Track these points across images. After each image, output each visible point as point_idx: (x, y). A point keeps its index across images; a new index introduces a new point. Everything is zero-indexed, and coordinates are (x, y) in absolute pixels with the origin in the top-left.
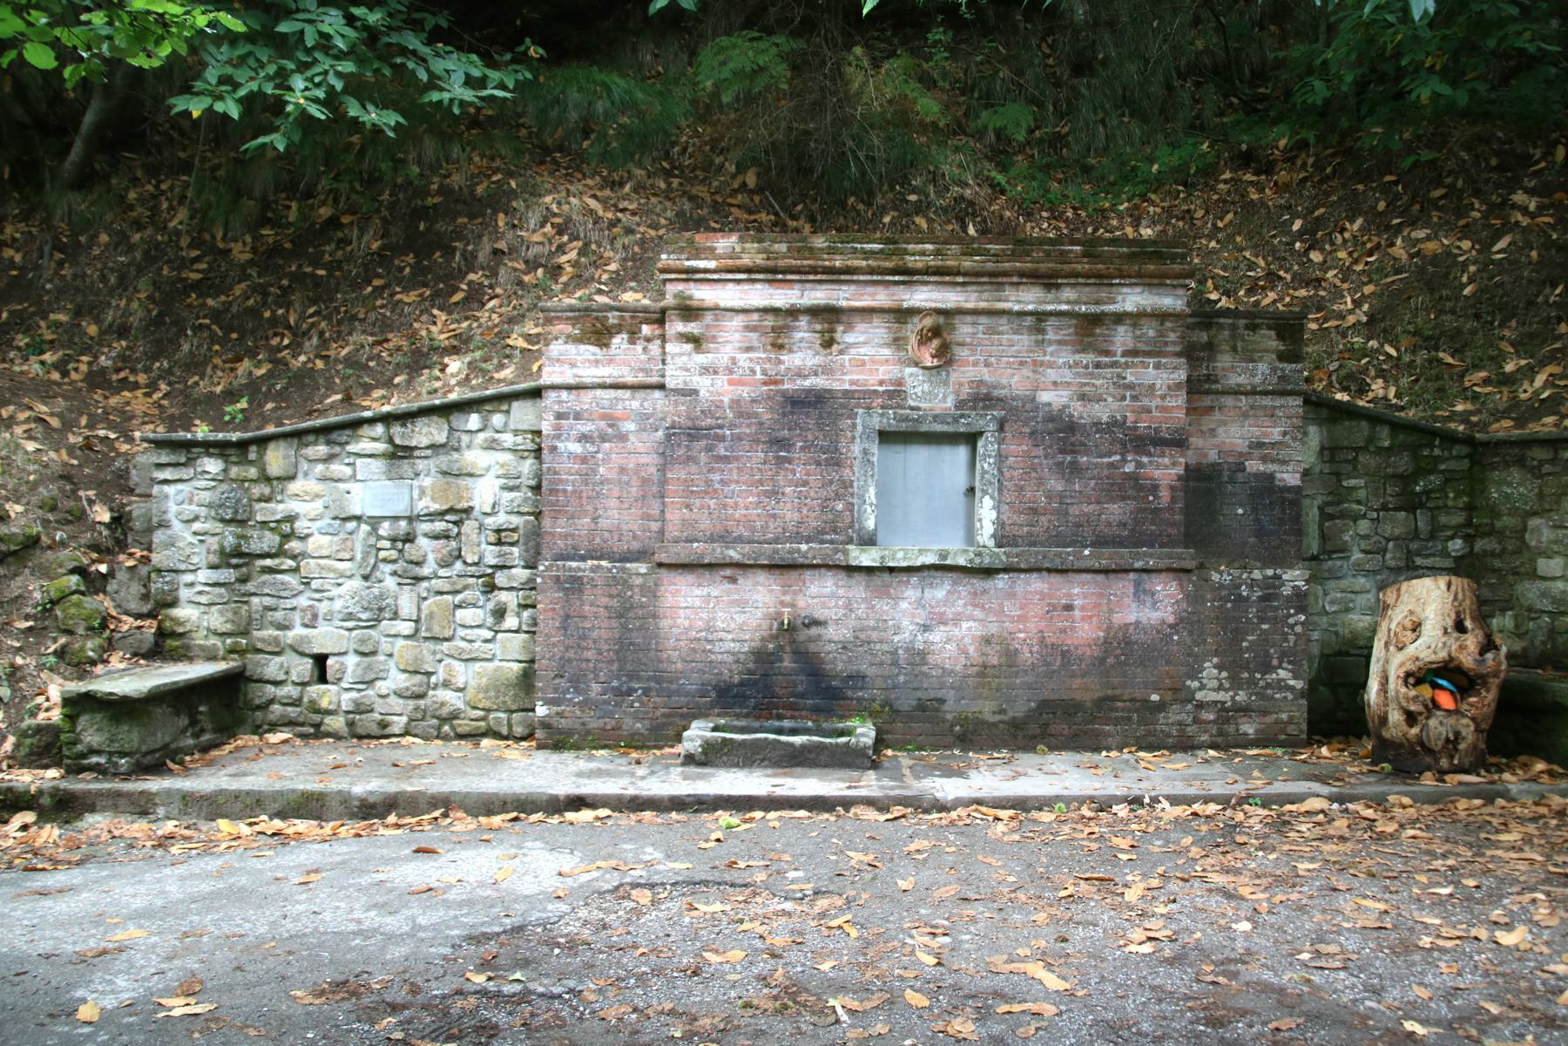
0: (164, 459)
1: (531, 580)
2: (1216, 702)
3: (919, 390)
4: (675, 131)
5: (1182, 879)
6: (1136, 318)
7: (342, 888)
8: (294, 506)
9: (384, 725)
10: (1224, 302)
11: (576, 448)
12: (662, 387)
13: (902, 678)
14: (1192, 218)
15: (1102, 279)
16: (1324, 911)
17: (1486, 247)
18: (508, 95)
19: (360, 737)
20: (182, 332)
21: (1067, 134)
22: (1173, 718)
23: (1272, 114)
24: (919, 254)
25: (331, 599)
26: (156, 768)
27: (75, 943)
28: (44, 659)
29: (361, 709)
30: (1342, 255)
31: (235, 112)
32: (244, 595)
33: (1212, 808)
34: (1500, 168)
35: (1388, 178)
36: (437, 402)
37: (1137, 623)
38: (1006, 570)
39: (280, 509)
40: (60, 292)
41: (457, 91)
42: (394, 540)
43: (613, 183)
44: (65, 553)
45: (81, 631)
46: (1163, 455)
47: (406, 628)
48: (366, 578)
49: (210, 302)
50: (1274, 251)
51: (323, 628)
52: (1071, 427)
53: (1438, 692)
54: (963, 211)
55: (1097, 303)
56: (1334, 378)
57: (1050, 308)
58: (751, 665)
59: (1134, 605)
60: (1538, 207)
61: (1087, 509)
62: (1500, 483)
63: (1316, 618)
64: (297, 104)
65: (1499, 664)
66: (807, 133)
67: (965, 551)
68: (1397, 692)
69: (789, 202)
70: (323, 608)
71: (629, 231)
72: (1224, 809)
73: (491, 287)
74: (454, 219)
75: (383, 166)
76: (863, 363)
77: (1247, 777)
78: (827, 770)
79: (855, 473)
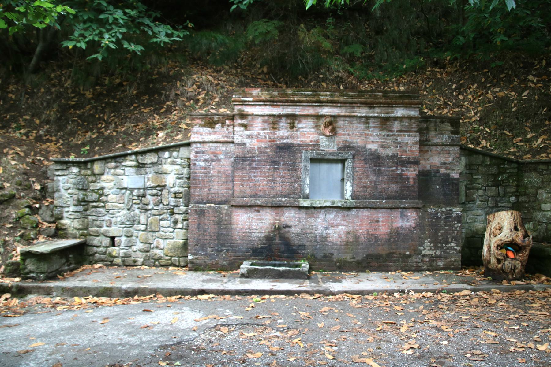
0: (58, 167)
1: (187, 211)
2: (429, 255)
3: (324, 144)
4: (239, 53)
5: (421, 323)
6: (401, 119)
7: (116, 325)
8: (103, 184)
9: (135, 261)
10: (429, 113)
11: (203, 164)
12: (233, 142)
13: (318, 246)
14: (418, 84)
15: (389, 105)
16: (473, 336)
17: (520, 95)
18: (180, 39)
19: (127, 266)
20: (68, 122)
21: (374, 55)
22: (414, 260)
23: (444, 49)
24: (325, 96)
25: (116, 217)
26: (54, 278)
27: (17, 348)
28: (16, 238)
29: (127, 256)
30: (470, 97)
31: (84, 46)
32: (86, 215)
33: (429, 294)
34: (524, 68)
35: (485, 70)
36: (154, 148)
37: (402, 227)
38: (355, 208)
39: (99, 185)
40: (27, 109)
41: (163, 38)
42: (138, 196)
43: (218, 71)
44: (24, 201)
45: (29, 228)
46: (411, 167)
47: (143, 227)
48: (129, 210)
49: (78, 112)
50: (446, 95)
51: (114, 227)
52: (378, 157)
53: (508, 252)
54: (338, 81)
55: (388, 113)
56: (468, 139)
57: (371, 115)
58: (265, 242)
59: (400, 220)
60: (537, 81)
61: (384, 186)
62: (528, 177)
63: (464, 224)
64: (106, 44)
65: (530, 242)
66: (285, 54)
67: (341, 201)
68: (494, 252)
69: (278, 77)
70: (114, 220)
71: (223, 87)
72: (434, 294)
73: (175, 107)
74: (162, 83)
75: (138, 65)
76: (305, 134)
77: (441, 283)
78: (291, 280)
79: (302, 173)
